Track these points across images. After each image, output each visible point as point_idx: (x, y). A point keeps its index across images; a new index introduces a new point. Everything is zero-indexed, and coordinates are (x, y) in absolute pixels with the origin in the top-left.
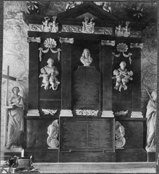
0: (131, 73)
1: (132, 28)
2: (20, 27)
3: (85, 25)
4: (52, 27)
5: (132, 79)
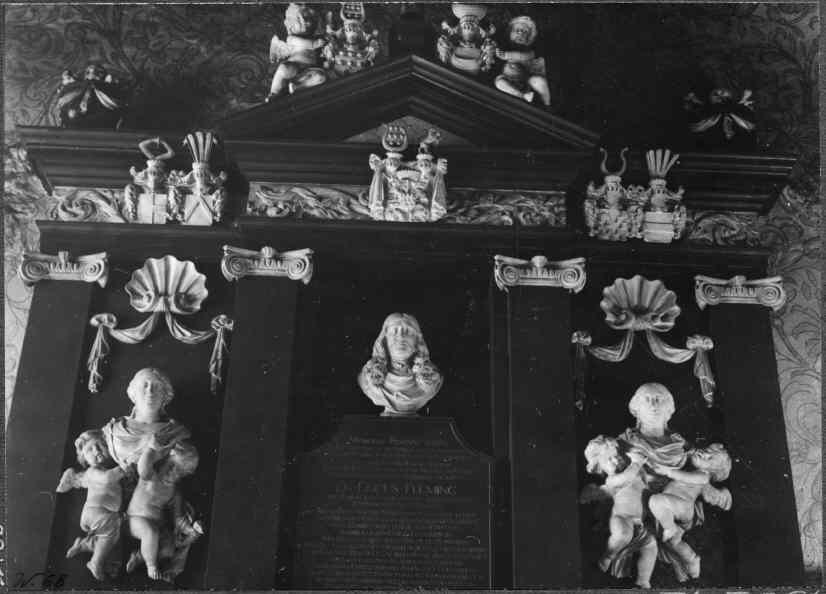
0: (716, 461)
1: (696, 189)
2: (16, 212)
3: (383, 170)
4: (189, 197)
5: (723, 499)
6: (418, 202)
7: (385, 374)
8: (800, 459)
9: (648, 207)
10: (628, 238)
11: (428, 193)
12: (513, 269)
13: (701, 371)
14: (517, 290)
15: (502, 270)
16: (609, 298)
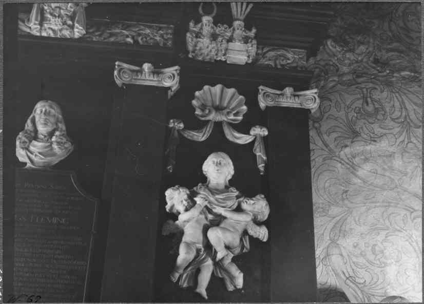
0: (259, 206)
5: (262, 233)
6: (64, 23)
7: (30, 141)
8: (324, 214)
9: (230, 40)
10: (215, 60)
11: (72, 18)
12: (128, 72)
13: (258, 150)
14: (130, 87)
15: (119, 71)
16: (198, 99)
